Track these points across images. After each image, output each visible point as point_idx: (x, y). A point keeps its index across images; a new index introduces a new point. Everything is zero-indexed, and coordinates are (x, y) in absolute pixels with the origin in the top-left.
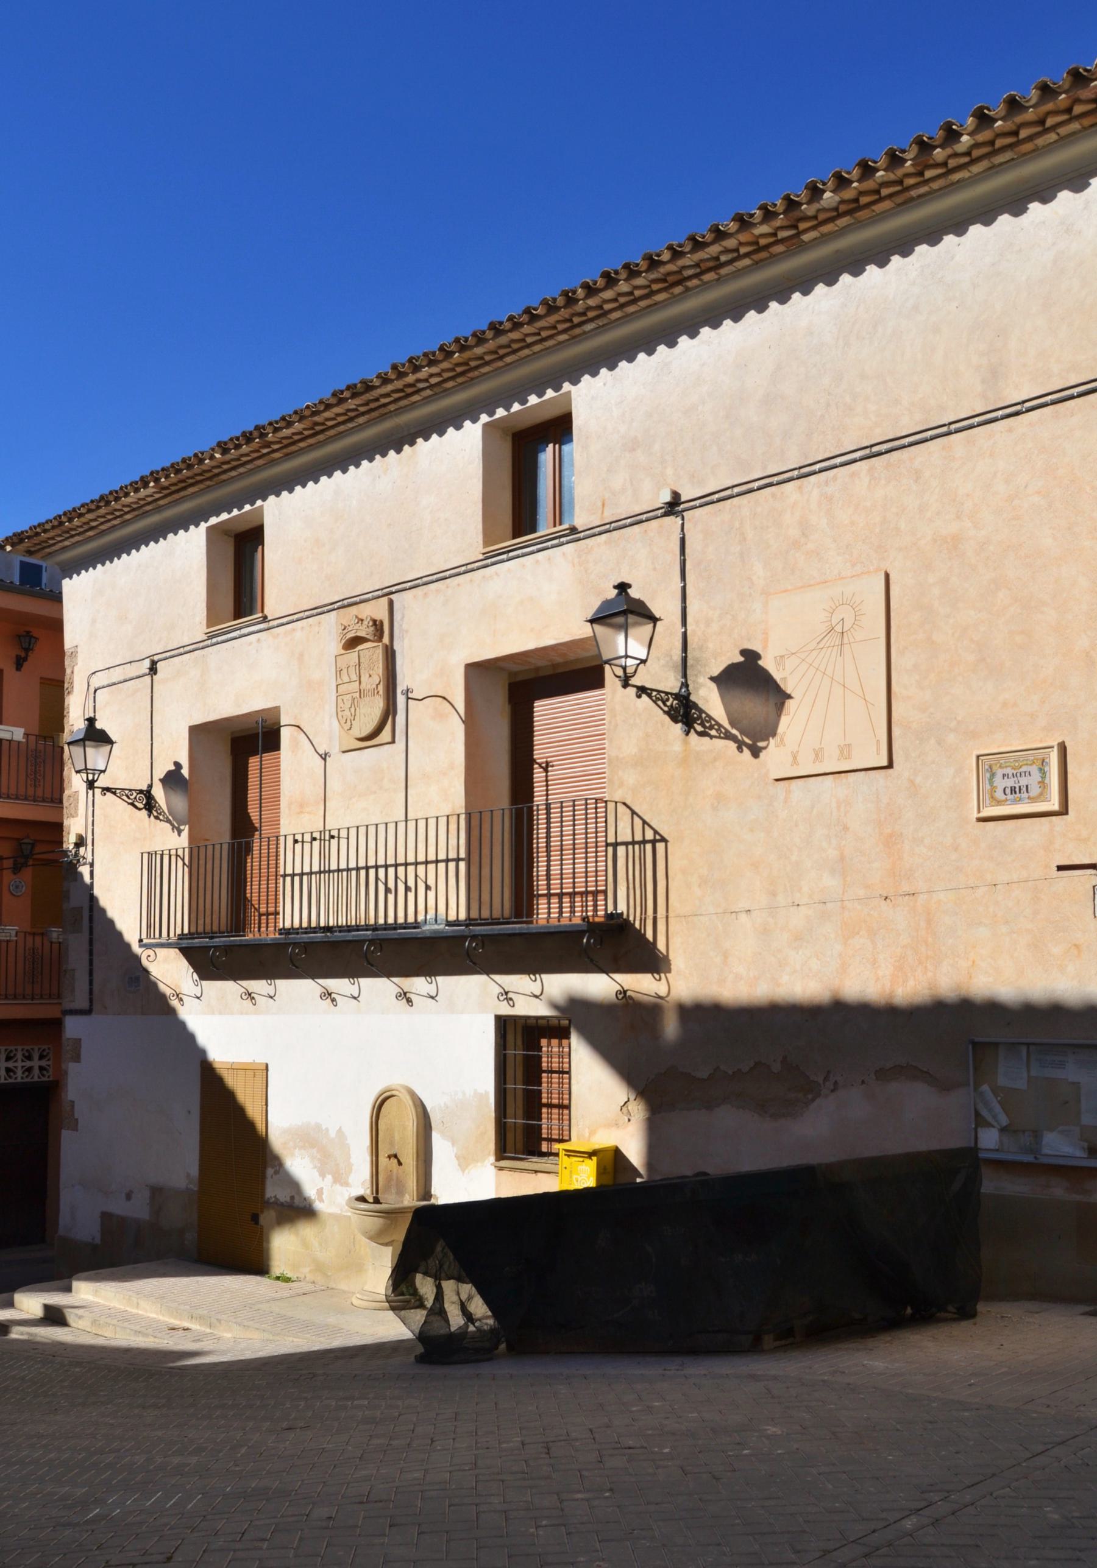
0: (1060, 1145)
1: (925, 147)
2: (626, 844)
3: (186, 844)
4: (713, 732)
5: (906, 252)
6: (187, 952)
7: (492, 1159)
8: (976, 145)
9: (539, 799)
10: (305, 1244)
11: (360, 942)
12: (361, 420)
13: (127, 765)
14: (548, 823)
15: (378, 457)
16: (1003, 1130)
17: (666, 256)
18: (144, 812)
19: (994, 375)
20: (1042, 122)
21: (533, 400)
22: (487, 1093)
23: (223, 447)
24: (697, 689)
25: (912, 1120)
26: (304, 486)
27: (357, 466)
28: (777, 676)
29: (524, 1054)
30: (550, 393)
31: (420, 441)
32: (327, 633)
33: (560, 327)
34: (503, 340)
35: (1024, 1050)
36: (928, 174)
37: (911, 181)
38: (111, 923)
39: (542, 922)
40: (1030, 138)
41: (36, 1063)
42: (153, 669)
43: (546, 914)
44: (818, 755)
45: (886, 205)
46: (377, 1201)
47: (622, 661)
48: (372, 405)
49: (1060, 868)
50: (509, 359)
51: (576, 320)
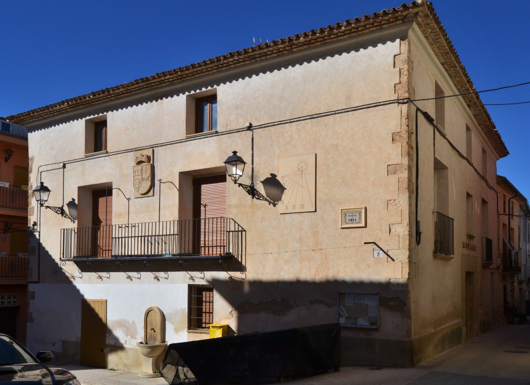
0: (362, 322)
1: (331, 29)
2: (233, 232)
3: (76, 226)
4: (261, 198)
5: (324, 58)
6: (76, 263)
7: (187, 329)
8: (346, 30)
9: (202, 217)
10: (120, 358)
11: (143, 260)
12: (144, 90)
13: (54, 199)
14: (205, 224)
15: (149, 102)
16: (346, 318)
17: (250, 50)
18: (61, 215)
19: (349, 98)
20: (365, 26)
21: (204, 89)
22: (185, 309)
23: (94, 94)
24: (256, 185)
25: (321, 316)
26: (122, 109)
27: (142, 104)
28: (282, 182)
29: (197, 296)
30: (209, 88)
31: (164, 98)
32: (131, 159)
33: (214, 68)
34: (195, 70)
35: (353, 295)
36: (332, 36)
37: (327, 38)
38: (47, 252)
39: (203, 255)
40: (361, 30)
41: (12, 300)
42: (64, 166)
43: (204, 253)
44: (294, 207)
45: (319, 43)
46: (146, 343)
47: (235, 176)
48: (149, 86)
49: (365, 243)
50: (196, 76)
51: (220, 66)
